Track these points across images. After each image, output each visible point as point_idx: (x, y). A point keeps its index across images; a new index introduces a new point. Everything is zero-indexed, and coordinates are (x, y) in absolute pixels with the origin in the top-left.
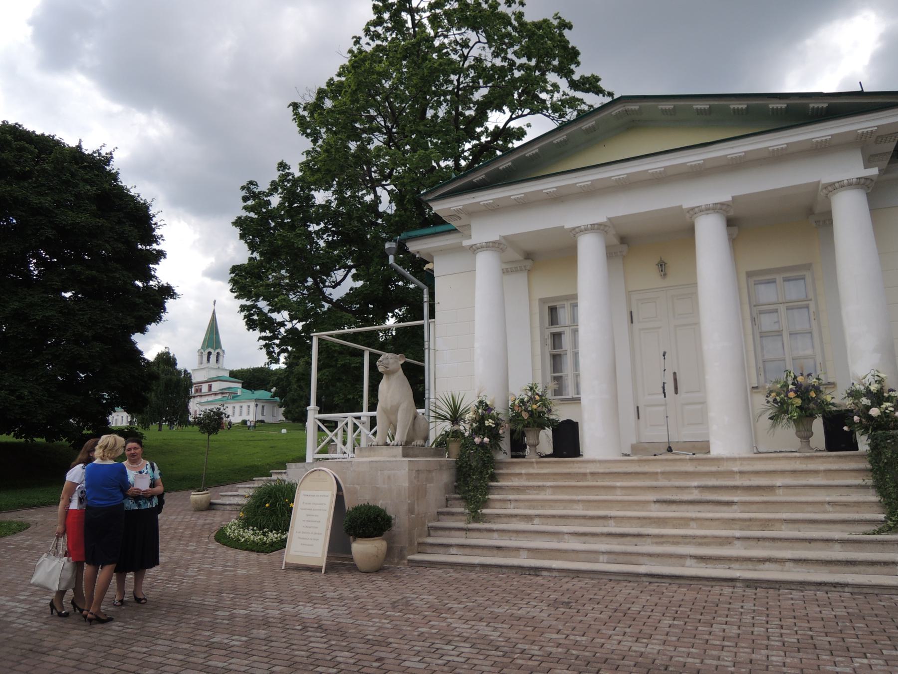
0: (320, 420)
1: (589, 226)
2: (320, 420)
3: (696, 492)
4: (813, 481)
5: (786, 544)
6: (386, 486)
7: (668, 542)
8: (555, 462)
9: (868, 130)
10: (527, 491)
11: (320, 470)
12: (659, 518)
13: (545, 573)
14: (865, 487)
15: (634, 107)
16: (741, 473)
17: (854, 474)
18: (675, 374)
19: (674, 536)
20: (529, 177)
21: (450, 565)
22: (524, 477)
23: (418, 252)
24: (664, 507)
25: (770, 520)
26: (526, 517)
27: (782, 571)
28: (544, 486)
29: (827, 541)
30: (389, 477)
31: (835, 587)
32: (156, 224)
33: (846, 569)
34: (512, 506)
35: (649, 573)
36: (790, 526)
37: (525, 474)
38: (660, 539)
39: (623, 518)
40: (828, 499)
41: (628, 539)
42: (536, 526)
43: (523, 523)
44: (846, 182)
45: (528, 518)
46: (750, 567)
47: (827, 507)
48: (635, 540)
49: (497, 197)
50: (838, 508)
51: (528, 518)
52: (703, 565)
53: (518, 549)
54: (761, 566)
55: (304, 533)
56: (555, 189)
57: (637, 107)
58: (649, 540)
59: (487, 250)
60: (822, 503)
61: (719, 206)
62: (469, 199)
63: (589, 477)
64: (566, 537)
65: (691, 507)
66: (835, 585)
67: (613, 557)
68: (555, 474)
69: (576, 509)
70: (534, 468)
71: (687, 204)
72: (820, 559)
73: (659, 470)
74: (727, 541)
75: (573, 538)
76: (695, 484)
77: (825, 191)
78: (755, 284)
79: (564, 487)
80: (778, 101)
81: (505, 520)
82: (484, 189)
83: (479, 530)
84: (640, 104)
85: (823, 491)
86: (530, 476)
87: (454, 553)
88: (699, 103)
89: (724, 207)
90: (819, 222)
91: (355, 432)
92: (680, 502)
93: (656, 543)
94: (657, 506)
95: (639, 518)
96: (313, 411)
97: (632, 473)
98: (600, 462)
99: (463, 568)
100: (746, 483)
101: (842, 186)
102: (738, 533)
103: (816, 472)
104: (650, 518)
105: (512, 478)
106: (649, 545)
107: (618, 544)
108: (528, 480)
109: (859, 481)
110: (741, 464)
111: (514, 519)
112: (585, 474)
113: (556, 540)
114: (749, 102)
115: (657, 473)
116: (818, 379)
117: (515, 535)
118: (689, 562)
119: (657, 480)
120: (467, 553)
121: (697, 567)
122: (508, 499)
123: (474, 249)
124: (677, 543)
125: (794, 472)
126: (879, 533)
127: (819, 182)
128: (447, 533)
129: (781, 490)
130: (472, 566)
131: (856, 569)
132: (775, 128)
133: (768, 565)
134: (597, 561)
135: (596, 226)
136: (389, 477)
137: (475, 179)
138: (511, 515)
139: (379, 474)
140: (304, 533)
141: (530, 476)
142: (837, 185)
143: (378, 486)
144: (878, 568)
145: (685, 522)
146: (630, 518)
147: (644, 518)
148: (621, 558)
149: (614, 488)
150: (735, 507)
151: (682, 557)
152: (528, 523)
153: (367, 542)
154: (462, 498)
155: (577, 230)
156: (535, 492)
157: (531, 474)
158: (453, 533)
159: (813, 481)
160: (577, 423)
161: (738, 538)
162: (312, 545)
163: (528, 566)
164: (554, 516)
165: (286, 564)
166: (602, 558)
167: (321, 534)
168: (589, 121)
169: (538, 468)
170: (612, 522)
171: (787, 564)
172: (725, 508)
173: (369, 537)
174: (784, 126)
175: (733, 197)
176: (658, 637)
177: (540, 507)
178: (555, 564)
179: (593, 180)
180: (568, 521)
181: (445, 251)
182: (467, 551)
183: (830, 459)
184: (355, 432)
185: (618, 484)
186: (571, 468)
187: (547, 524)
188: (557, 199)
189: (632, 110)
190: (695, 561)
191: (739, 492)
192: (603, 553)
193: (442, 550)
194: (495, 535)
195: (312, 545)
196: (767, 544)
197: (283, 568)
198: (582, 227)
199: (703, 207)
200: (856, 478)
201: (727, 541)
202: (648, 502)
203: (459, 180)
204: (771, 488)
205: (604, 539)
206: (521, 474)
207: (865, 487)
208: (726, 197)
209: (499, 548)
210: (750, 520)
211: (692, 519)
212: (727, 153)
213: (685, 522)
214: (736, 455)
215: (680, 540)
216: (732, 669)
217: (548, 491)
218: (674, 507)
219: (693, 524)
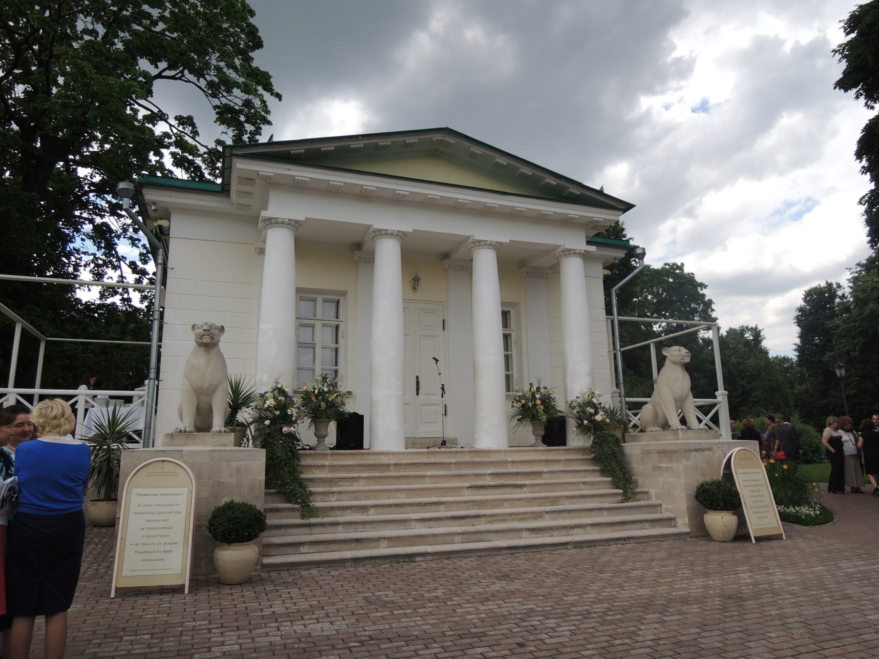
0: (20, 395)
1: (287, 220)
2: (20, 395)
3: (489, 478)
4: (556, 468)
5: (577, 514)
6: (234, 480)
7: (498, 520)
8: (351, 454)
9: (370, 188)
10: (340, 483)
11: (163, 461)
12: (481, 501)
13: (419, 559)
14: (593, 471)
15: (452, 140)
16: (513, 462)
17: (581, 462)
18: (417, 377)
19: (504, 514)
20: (341, 167)
21: (317, 564)
22: (327, 470)
23: (154, 203)
24: (475, 491)
25: (557, 497)
26: (361, 509)
27: (584, 534)
28: (359, 478)
29: (600, 509)
30: (238, 470)
31: (625, 540)
32: (864, 215)
33: (620, 528)
34: (334, 499)
35: (509, 546)
36: (570, 501)
37: (328, 466)
38: (493, 518)
39: (452, 502)
40: (583, 480)
41: (467, 520)
42: (372, 516)
43: (358, 514)
44: (578, 251)
45: (364, 509)
46: (565, 533)
47: (582, 486)
48: (472, 521)
49: (316, 177)
50: (588, 486)
51: (364, 509)
52: (534, 535)
53: (378, 539)
54: (572, 532)
55: (144, 544)
56: (375, 189)
57: (454, 142)
58: (483, 520)
59: (287, 227)
60: (579, 483)
61: (401, 234)
62: (283, 169)
63: (392, 468)
64: (413, 523)
65: (494, 491)
66: (625, 539)
67: (466, 536)
68: (359, 466)
69: (399, 498)
70: (327, 460)
71: (378, 224)
72: (607, 522)
73: (454, 461)
74: (538, 515)
75: (419, 524)
76: (490, 471)
77: (472, 245)
78: (300, 300)
79: (379, 477)
80: (553, 178)
81: (338, 512)
82: (279, 161)
83: (323, 525)
84: (457, 140)
85: (570, 475)
86: (333, 468)
87: (305, 551)
88: (502, 158)
89: (297, 225)
90: (528, 272)
91: (717, 414)
92: (488, 486)
93: (489, 522)
94: (469, 491)
95: (466, 502)
96: (721, 396)
97: (431, 463)
98: (394, 454)
99: (331, 565)
100: (457, 472)
101: (575, 253)
102: (548, 508)
103: (559, 461)
104: (474, 501)
105: (314, 470)
106: (483, 524)
107: (459, 526)
108: (331, 471)
109: (591, 468)
110: (505, 456)
111: (348, 511)
112: (388, 465)
113: (404, 528)
114: (535, 172)
115: (451, 464)
116: (341, 386)
117: (361, 526)
118: (525, 534)
119: (450, 470)
120: (321, 550)
121: (530, 538)
122: (332, 491)
123: (271, 222)
124: (504, 521)
125: (546, 461)
126: (622, 502)
127: (469, 237)
128: (283, 531)
129: (546, 475)
130: (342, 562)
131: (625, 527)
132: (538, 196)
133: (576, 530)
134: (452, 543)
135: (401, 234)
136: (238, 470)
137: (293, 150)
138: (346, 507)
139: (224, 466)
140: (144, 544)
141: (333, 468)
142: (273, 221)
143: (222, 480)
144: (636, 525)
145: (500, 503)
146: (459, 502)
147: (470, 502)
148: (472, 537)
149: (424, 477)
150: (525, 489)
151: (520, 530)
152: (363, 514)
153: (243, 547)
154: (278, 493)
155: (383, 232)
156: (349, 484)
157: (335, 466)
158: (290, 531)
159: (556, 468)
160: (362, 416)
161: (548, 512)
162: (766, 517)
163: (405, 553)
164: (390, 506)
165: (117, 589)
166: (458, 539)
167: (768, 506)
168: (413, 137)
169: (331, 460)
170: (442, 507)
171: (588, 528)
172: (518, 490)
173: (243, 542)
174: (541, 196)
175: (306, 218)
176: (122, 648)
177: (364, 498)
178: (430, 549)
179: (277, 174)
180: (403, 509)
181: (186, 210)
182: (321, 548)
183: (560, 452)
184: (717, 414)
185: (429, 473)
186: (366, 459)
187: (382, 514)
188: (365, 197)
189: (448, 142)
190: (529, 532)
191: (519, 477)
192: (459, 534)
193: (289, 550)
194: (340, 528)
195: (766, 517)
196: (565, 515)
197: (112, 595)
198: (280, 219)
199: (390, 231)
200: (582, 465)
201: (538, 515)
202: (462, 488)
203: (277, 146)
204: (539, 474)
205: (446, 522)
206: (324, 466)
207: (593, 471)
208: (505, 239)
209: (358, 540)
210: (546, 498)
211: (506, 500)
212: (363, 184)
213: (500, 503)
214: (502, 448)
215: (507, 517)
216: (254, 655)
217: (362, 482)
218: (482, 491)
219: (506, 504)
